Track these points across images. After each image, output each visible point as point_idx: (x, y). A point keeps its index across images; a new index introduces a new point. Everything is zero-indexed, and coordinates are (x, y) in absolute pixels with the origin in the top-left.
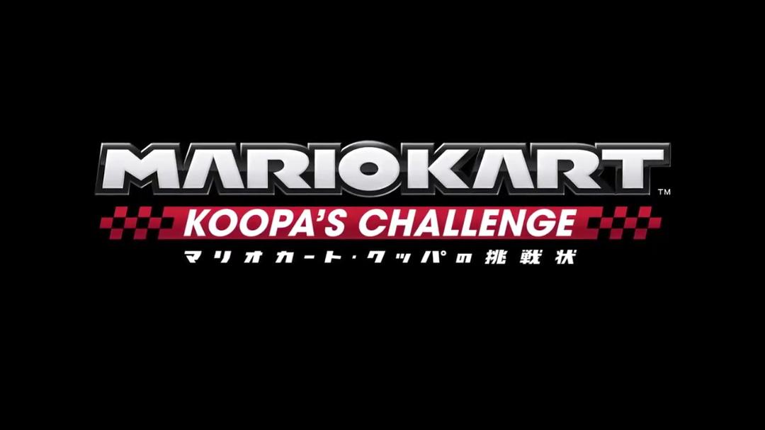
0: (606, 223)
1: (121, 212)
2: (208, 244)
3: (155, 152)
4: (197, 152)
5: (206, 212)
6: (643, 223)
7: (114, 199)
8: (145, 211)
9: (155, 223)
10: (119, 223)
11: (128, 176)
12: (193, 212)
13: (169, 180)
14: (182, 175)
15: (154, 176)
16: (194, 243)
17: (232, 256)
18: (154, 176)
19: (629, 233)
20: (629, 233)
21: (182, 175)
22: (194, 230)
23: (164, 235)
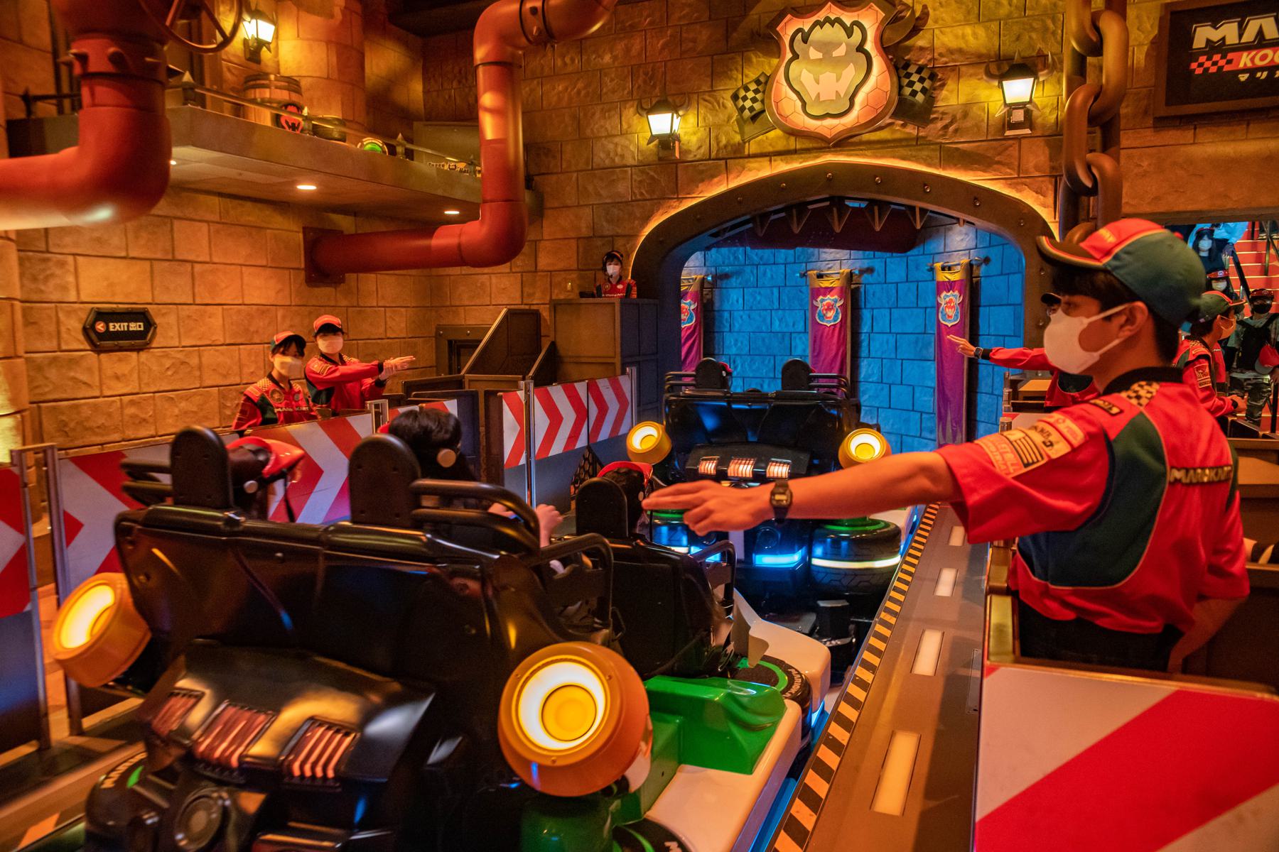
0: (1222, 63)
1: (1202, 59)
2: (1252, 71)
3: (1225, 25)
4: (1198, 29)
5: (1254, 53)
6: (1201, 65)
7: (1201, 52)
8: (1216, 57)
9: (1222, 63)
10: (1201, 65)
11: (1208, 41)
12: (1245, 54)
13: (1232, 39)
14: (1241, 36)
15: (1223, 39)
16: (1244, 71)
17: (1268, 74)
18: (1223, 39)
19: (1207, 70)
20: (1207, 70)
21: (1241, 36)
22: (1245, 64)
23: (1227, 68)
